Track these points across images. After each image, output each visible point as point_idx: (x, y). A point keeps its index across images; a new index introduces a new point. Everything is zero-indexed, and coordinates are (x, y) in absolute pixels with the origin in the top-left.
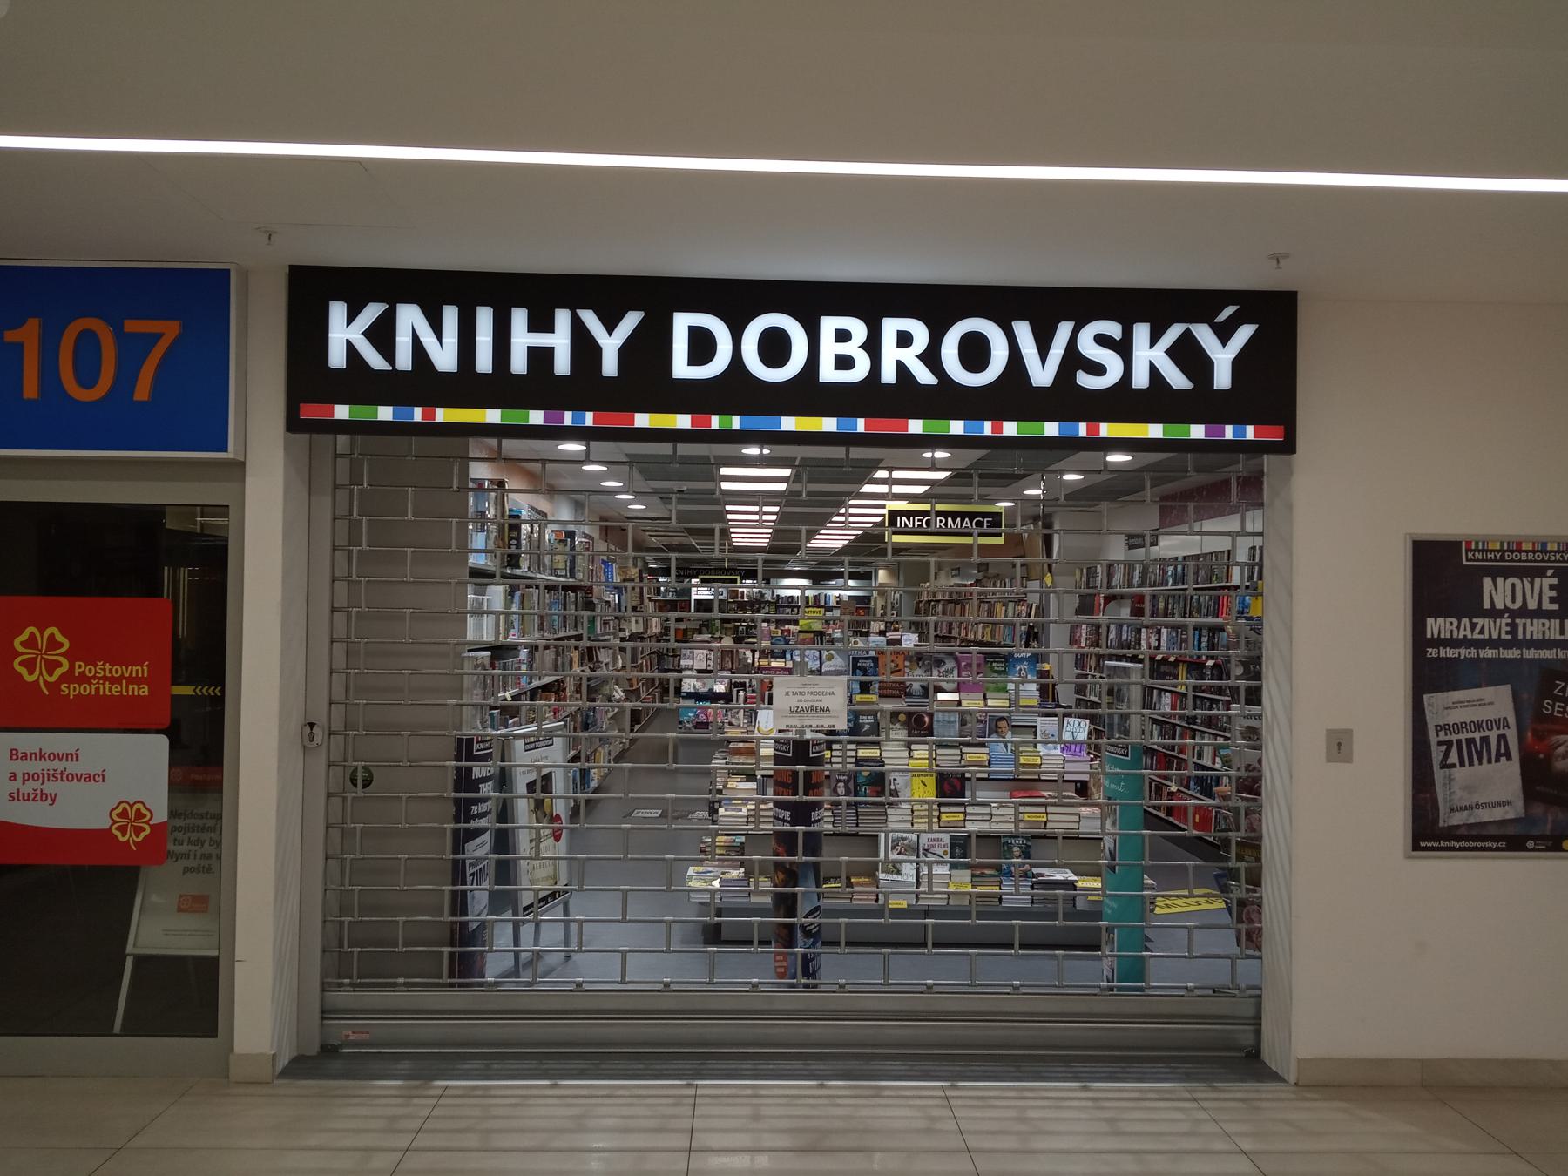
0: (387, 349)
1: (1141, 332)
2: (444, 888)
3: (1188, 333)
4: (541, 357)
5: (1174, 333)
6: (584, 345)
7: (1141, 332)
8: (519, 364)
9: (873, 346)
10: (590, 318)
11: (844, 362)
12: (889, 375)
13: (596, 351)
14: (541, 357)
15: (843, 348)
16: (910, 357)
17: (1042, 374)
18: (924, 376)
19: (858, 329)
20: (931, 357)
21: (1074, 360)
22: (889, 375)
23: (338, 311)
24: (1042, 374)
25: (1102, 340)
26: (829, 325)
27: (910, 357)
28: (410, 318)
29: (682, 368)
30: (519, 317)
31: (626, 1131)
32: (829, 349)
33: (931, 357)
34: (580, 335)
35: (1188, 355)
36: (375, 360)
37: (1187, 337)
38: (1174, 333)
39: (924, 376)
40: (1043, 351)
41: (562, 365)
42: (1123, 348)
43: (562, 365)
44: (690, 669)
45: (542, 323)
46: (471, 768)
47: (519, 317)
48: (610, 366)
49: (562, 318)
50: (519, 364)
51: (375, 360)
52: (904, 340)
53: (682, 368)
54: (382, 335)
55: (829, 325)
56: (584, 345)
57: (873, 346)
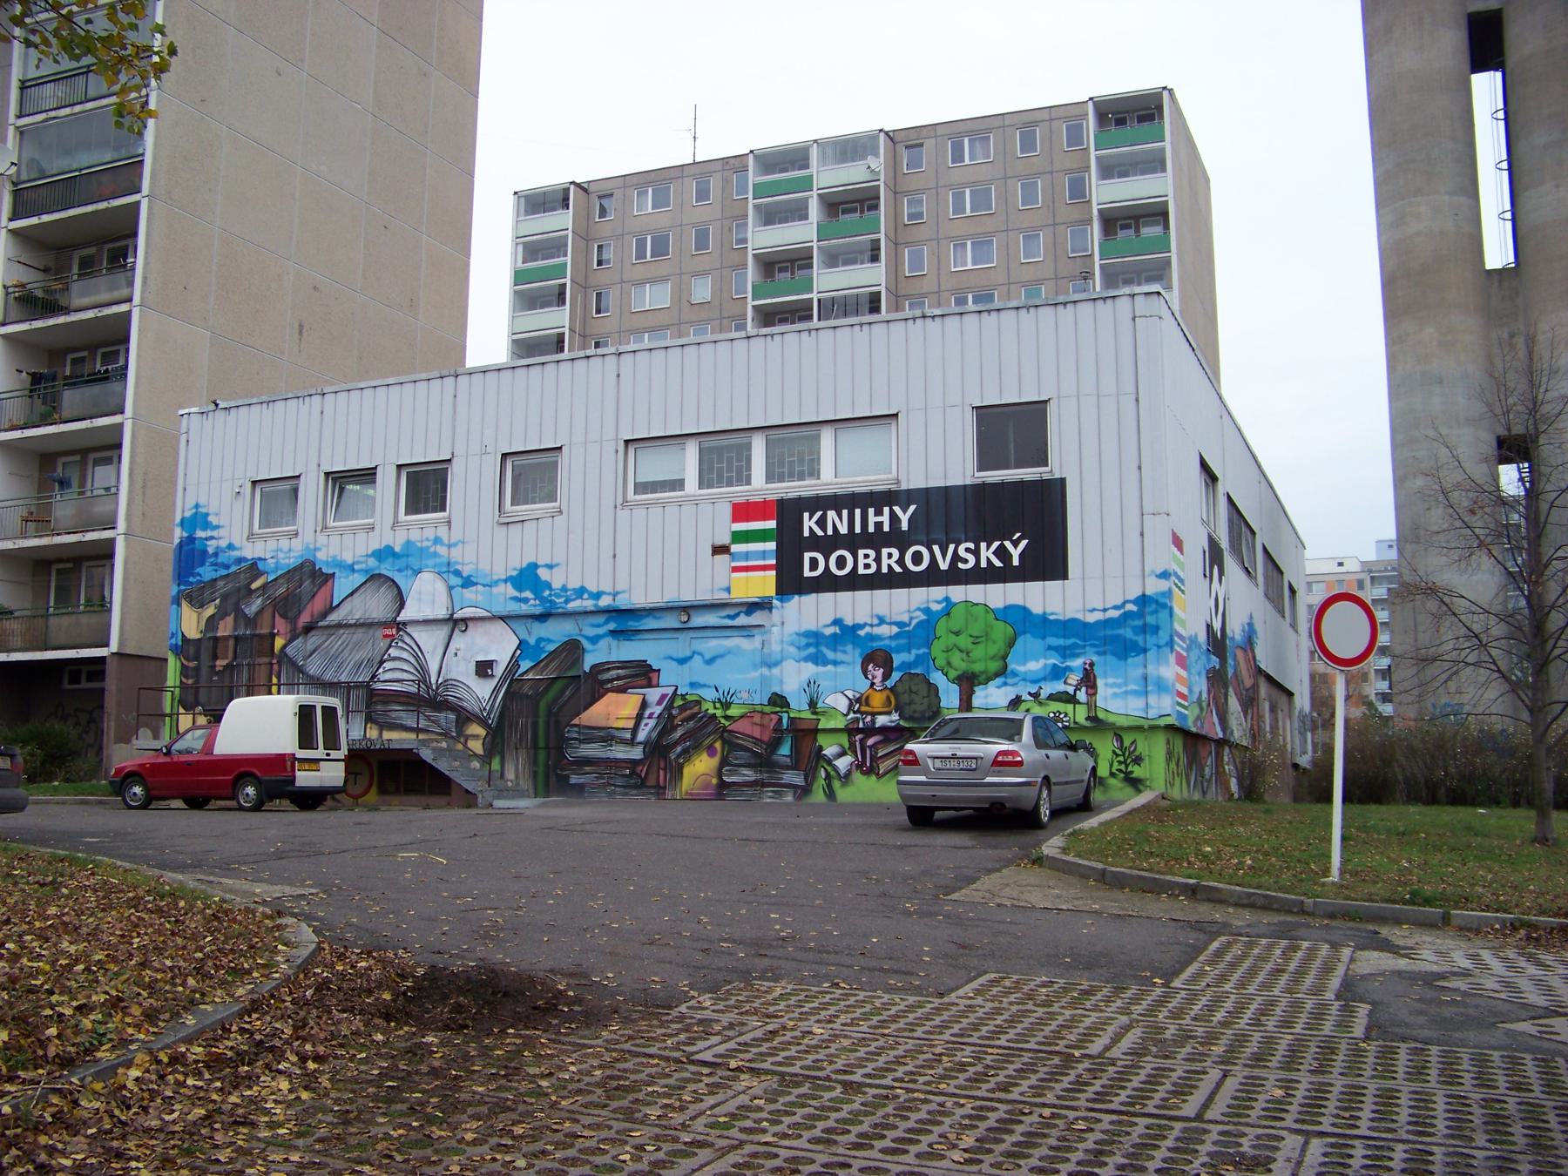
0: (824, 529)
1: (983, 545)
2: (119, 863)
3: (1002, 545)
4: (879, 525)
5: (996, 544)
6: (894, 519)
7: (983, 545)
8: (871, 529)
9: (878, 560)
10: (897, 509)
11: (867, 566)
12: (885, 570)
13: (899, 521)
14: (879, 525)
15: (867, 561)
16: (892, 562)
17: (944, 565)
18: (898, 569)
19: (872, 553)
20: (901, 562)
21: (956, 558)
22: (885, 570)
23: (806, 515)
24: (944, 565)
25: (967, 550)
26: (861, 552)
27: (892, 562)
28: (831, 514)
29: (807, 573)
30: (871, 511)
31: (1468, 1155)
32: (861, 561)
33: (901, 562)
34: (893, 515)
35: (1002, 553)
36: (820, 533)
37: (1002, 547)
38: (996, 544)
39: (898, 569)
40: (944, 556)
41: (886, 528)
42: (976, 553)
43: (886, 528)
44: (623, 741)
45: (879, 513)
46: (960, 710)
47: (871, 511)
48: (905, 526)
49: (886, 510)
50: (871, 529)
51: (820, 533)
52: (890, 556)
53: (807, 573)
54: (822, 523)
55: (861, 552)
56: (894, 519)
57: (878, 560)
